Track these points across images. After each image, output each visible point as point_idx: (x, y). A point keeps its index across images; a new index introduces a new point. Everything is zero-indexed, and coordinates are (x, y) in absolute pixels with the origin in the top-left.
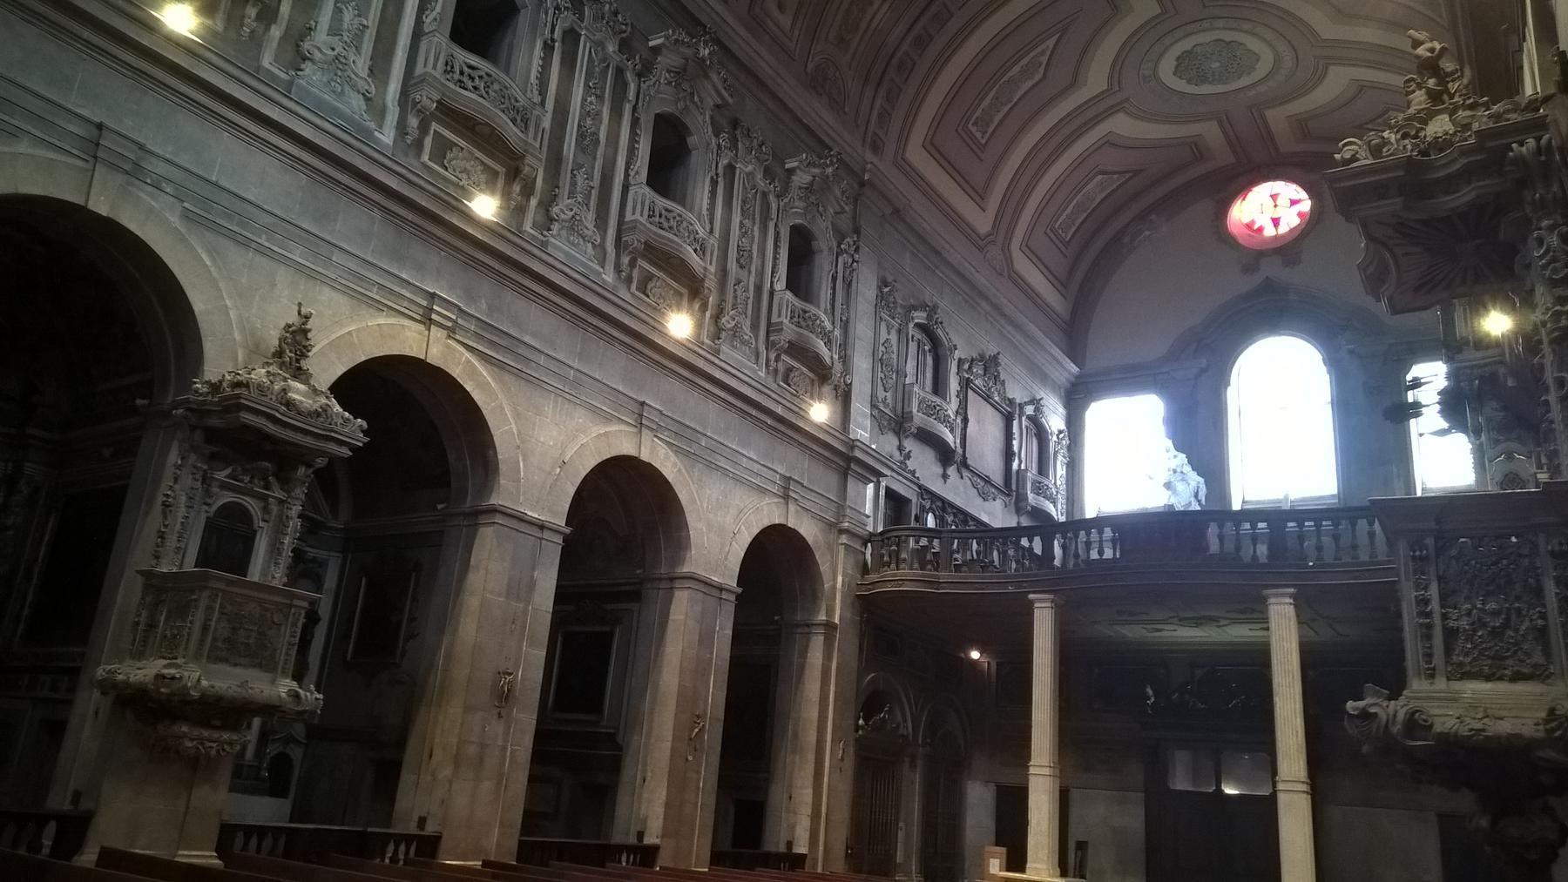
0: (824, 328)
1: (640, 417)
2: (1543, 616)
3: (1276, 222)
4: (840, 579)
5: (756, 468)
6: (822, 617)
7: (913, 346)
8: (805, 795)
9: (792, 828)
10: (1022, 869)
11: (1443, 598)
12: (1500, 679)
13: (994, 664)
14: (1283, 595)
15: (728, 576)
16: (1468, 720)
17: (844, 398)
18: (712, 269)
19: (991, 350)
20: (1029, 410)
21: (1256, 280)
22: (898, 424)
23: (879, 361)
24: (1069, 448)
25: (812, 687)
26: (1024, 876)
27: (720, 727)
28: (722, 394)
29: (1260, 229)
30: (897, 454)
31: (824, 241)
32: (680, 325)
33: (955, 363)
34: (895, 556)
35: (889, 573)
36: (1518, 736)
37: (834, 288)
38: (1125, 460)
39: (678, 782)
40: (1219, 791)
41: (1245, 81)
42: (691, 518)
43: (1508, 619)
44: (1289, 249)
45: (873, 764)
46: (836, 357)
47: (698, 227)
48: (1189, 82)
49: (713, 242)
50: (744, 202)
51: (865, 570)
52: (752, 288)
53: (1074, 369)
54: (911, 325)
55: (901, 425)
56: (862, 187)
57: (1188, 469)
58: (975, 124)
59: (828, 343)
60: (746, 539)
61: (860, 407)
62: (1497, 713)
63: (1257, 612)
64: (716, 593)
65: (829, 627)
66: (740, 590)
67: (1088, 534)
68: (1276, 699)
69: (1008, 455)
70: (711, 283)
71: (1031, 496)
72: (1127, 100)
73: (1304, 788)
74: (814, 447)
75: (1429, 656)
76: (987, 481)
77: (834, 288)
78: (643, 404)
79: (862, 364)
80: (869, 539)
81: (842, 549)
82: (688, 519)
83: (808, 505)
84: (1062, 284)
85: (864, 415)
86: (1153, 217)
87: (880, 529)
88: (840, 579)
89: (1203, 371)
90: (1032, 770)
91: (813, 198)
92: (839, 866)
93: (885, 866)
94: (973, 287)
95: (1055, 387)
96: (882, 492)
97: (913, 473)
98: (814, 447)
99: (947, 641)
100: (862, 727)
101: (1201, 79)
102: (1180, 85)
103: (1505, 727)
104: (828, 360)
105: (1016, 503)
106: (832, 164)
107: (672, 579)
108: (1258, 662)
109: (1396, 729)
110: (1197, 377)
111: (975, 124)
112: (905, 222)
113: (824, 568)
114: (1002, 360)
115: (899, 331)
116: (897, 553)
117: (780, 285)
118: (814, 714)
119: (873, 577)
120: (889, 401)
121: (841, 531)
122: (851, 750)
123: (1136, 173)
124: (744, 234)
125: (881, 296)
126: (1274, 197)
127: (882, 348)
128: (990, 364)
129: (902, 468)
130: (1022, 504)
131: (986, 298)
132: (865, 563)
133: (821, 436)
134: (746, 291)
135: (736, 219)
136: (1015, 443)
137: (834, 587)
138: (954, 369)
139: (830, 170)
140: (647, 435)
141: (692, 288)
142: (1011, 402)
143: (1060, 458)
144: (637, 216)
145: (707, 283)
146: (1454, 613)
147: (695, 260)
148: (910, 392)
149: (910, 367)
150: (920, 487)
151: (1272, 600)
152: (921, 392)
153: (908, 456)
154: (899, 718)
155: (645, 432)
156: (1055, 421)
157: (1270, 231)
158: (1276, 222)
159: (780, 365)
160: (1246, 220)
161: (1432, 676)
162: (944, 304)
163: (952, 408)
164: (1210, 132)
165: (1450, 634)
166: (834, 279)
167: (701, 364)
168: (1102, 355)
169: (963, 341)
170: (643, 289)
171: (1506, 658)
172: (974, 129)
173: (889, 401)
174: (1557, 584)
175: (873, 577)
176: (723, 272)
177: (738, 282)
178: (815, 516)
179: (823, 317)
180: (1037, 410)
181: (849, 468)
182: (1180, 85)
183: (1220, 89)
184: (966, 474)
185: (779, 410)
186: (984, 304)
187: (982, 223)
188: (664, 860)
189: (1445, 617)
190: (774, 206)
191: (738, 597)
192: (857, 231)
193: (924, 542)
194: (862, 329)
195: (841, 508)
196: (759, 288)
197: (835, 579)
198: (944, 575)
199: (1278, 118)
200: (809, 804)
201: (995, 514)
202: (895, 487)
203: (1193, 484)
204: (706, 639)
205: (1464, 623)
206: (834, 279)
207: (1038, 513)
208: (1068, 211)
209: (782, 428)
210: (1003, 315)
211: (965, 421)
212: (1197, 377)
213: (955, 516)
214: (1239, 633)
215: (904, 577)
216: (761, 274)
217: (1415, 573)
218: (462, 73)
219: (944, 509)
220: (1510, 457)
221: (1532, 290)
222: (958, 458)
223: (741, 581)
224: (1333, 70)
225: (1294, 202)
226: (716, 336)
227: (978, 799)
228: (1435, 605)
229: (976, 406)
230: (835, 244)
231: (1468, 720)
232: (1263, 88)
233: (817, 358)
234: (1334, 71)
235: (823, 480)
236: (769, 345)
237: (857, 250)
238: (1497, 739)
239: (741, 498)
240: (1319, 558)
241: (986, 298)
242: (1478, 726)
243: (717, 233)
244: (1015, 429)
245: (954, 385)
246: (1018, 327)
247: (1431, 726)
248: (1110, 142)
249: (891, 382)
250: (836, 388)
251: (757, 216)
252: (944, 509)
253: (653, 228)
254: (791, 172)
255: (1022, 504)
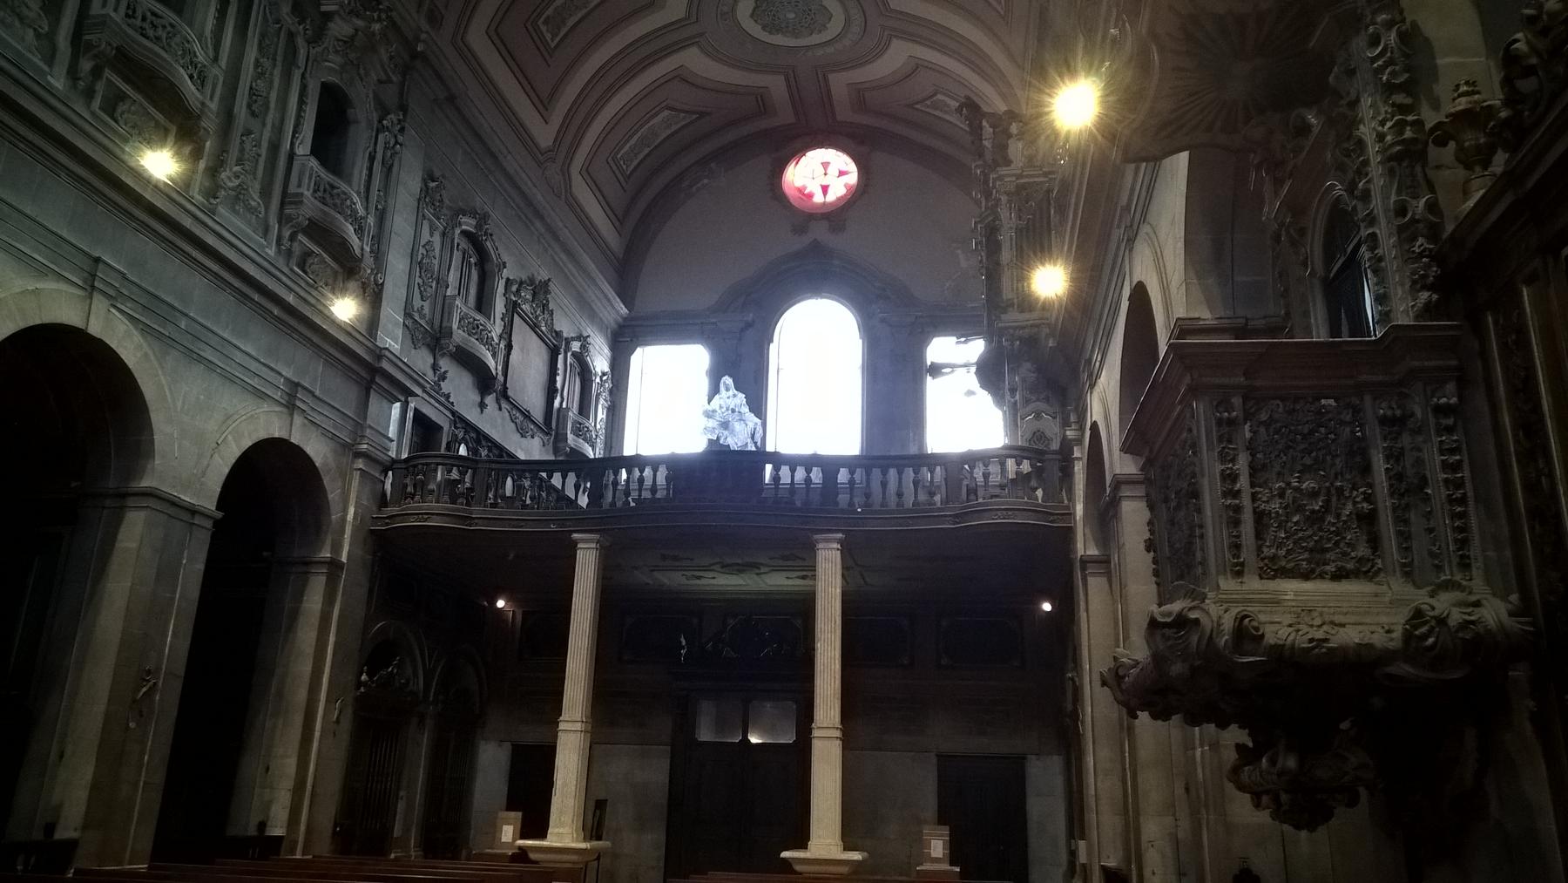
0: (355, 211)
1: (92, 278)
2: (1368, 498)
3: (825, 189)
4: (352, 511)
5: (254, 366)
6: (326, 554)
7: (457, 255)
8: (287, 765)
9: (267, 806)
10: (542, 835)
11: (1254, 470)
12: (1321, 576)
13: (519, 617)
14: (834, 540)
15: (205, 492)
16: (1305, 629)
17: (373, 297)
18: (213, 106)
19: (543, 275)
20: (576, 346)
21: (806, 240)
22: (435, 339)
23: (418, 264)
24: (611, 392)
25: (306, 636)
26: (545, 843)
27: (178, 685)
28: (215, 267)
29: (810, 196)
30: (430, 373)
31: (362, 110)
32: (160, 164)
33: (502, 284)
34: (421, 486)
35: (414, 505)
36: (1370, 646)
37: (370, 169)
38: (668, 405)
39: (112, 755)
40: (746, 740)
41: (816, 39)
42: (157, 418)
43: (1327, 502)
44: (837, 216)
45: (375, 723)
46: (367, 249)
47: (197, 47)
48: (764, 28)
49: (217, 73)
50: (263, 36)
51: (383, 501)
52: (265, 144)
53: (624, 311)
54: (458, 231)
55: (438, 340)
56: (413, 59)
57: (746, 409)
58: (546, 22)
59: (360, 231)
60: (233, 452)
61: (392, 314)
62: (1338, 619)
63: (801, 557)
64: (186, 516)
65: (334, 566)
66: (220, 515)
67: (642, 471)
68: (818, 645)
69: (551, 391)
70: (210, 124)
71: (570, 436)
72: (701, 35)
73: (838, 734)
74: (332, 351)
75: (1236, 547)
76: (527, 416)
77: (370, 169)
78: (97, 260)
79: (397, 265)
80: (392, 465)
81: (357, 475)
82: (153, 416)
83: (318, 419)
84: (619, 219)
85: (396, 324)
86: (713, 165)
87: (405, 456)
88: (352, 511)
89: (749, 325)
90: (562, 726)
91: (352, 56)
92: (324, 847)
93: (378, 844)
94: (530, 203)
95: (602, 327)
96: (410, 414)
97: (448, 396)
98: (332, 351)
99: (479, 588)
100: (365, 684)
101: (772, 28)
102: (755, 30)
103: (1351, 636)
104: (358, 251)
105: (555, 443)
106: (380, 20)
107: (124, 496)
108: (804, 607)
109: (1223, 640)
110: (742, 330)
111: (546, 22)
112: (458, 109)
113: (333, 495)
114: (551, 286)
115: (444, 234)
116: (423, 484)
117: (303, 149)
118: (307, 668)
119: (392, 510)
120: (426, 310)
121: (358, 455)
122: (349, 711)
123: (702, 115)
124: (260, 75)
125: (426, 190)
126: (825, 165)
127: (422, 250)
128: (540, 291)
129: (436, 392)
130: (561, 445)
131: (542, 218)
132: (384, 494)
133: (343, 338)
134: (258, 145)
135: (251, 54)
136: (559, 379)
137: (344, 519)
138: (501, 289)
139: (377, 27)
140: (100, 304)
141: (180, 124)
142: (558, 334)
143: (602, 401)
144: (109, 10)
145: (204, 123)
146: (1264, 494)
147: (189, 88)
148: (451, 306)
149: (453, 278)
150: (453, 413)
151: (820, 546)
152: (463, 307)
153: (443, 377)
154: (409, 671)
155: (97, 297)
156: (600, 363)
157: (819, 198)
158: (825, 189)
159: (296, 244)
160: (798, 184)
161: (1239, 574)
162: (495, 215)
163: (496, 329)
164: (776, 86)
165: (1260, 517)
166: (372, 159)
167: (187, 222)
168: (656, 296)
169: (515, 260)
170: (110, 107)
171: (1327, 550)
172: (544, 28)
173: (426, 310)
174: (1387, 458)
175: (392, 510)
176: (228, 116)
177: (248, 132)
178: (325, 433)
179: (356, 198)
180: (584, 347)
181: (373, 381)
182: (755, 30)
183: (792, 42)
184: (504, 405)
185: (290, 299)
186: (538, 224)
187: (544, 135)
188: (82, 861)
189: (1254, 497)
190: (302, 52)
191: (217, 523)
192: (403, 108)
193: (455, 475)
194: (402, 224)
195: (359, 426)
196: (274, 147)
197: (345, 511)
198: (477, 511)
199: (839, 82)
200: (291, 777)
201: (530, 449)
202: (427, 411)
203: (751, 425)
204: (167, 572)
205: (1275, 505)
206: (372, 159)
207: (577, 454)
208: (632, 142)
209: (293, 322)
210: (556, 238)
211: (509, 347)
212: (742, 330)
213: (490, 450)
214: (779, 581)
215: (431, 511)
216: (279, 129)
217: (1220, 439)
218: (144, 19)
219: (478, 442)
220: (1038, 416)
221: (1357, 101)
222: (499, 387)
223: (222, 502)
224: (895, 43)
225: (842, 173)
226: (211, 193)
227: (492, 762)
228: (1243, 483)
229: (521, 332)
230: (375, 117)
231: (1305, 629)
232: (830, 50)
233: (344, 245)
234: (896, 44)
235: (344, 394)
236: (283, 219)
237: (402, 130)
238: (1343, 649)
239: (232, 402)
240: (867, 505)
241: (542, 218)
242: (1320, 635)
243: (223, 62)
244: (560, 365)
245: (500, 306)
246: (569, 253)
247: (1262, 636)
248: (681, 77)
249: (430, 291)
250: (364, 286)
251: (279, 59)
252: (478, 442)
253: (130, 31)
254: (328, 16)
255: (561, 445)
